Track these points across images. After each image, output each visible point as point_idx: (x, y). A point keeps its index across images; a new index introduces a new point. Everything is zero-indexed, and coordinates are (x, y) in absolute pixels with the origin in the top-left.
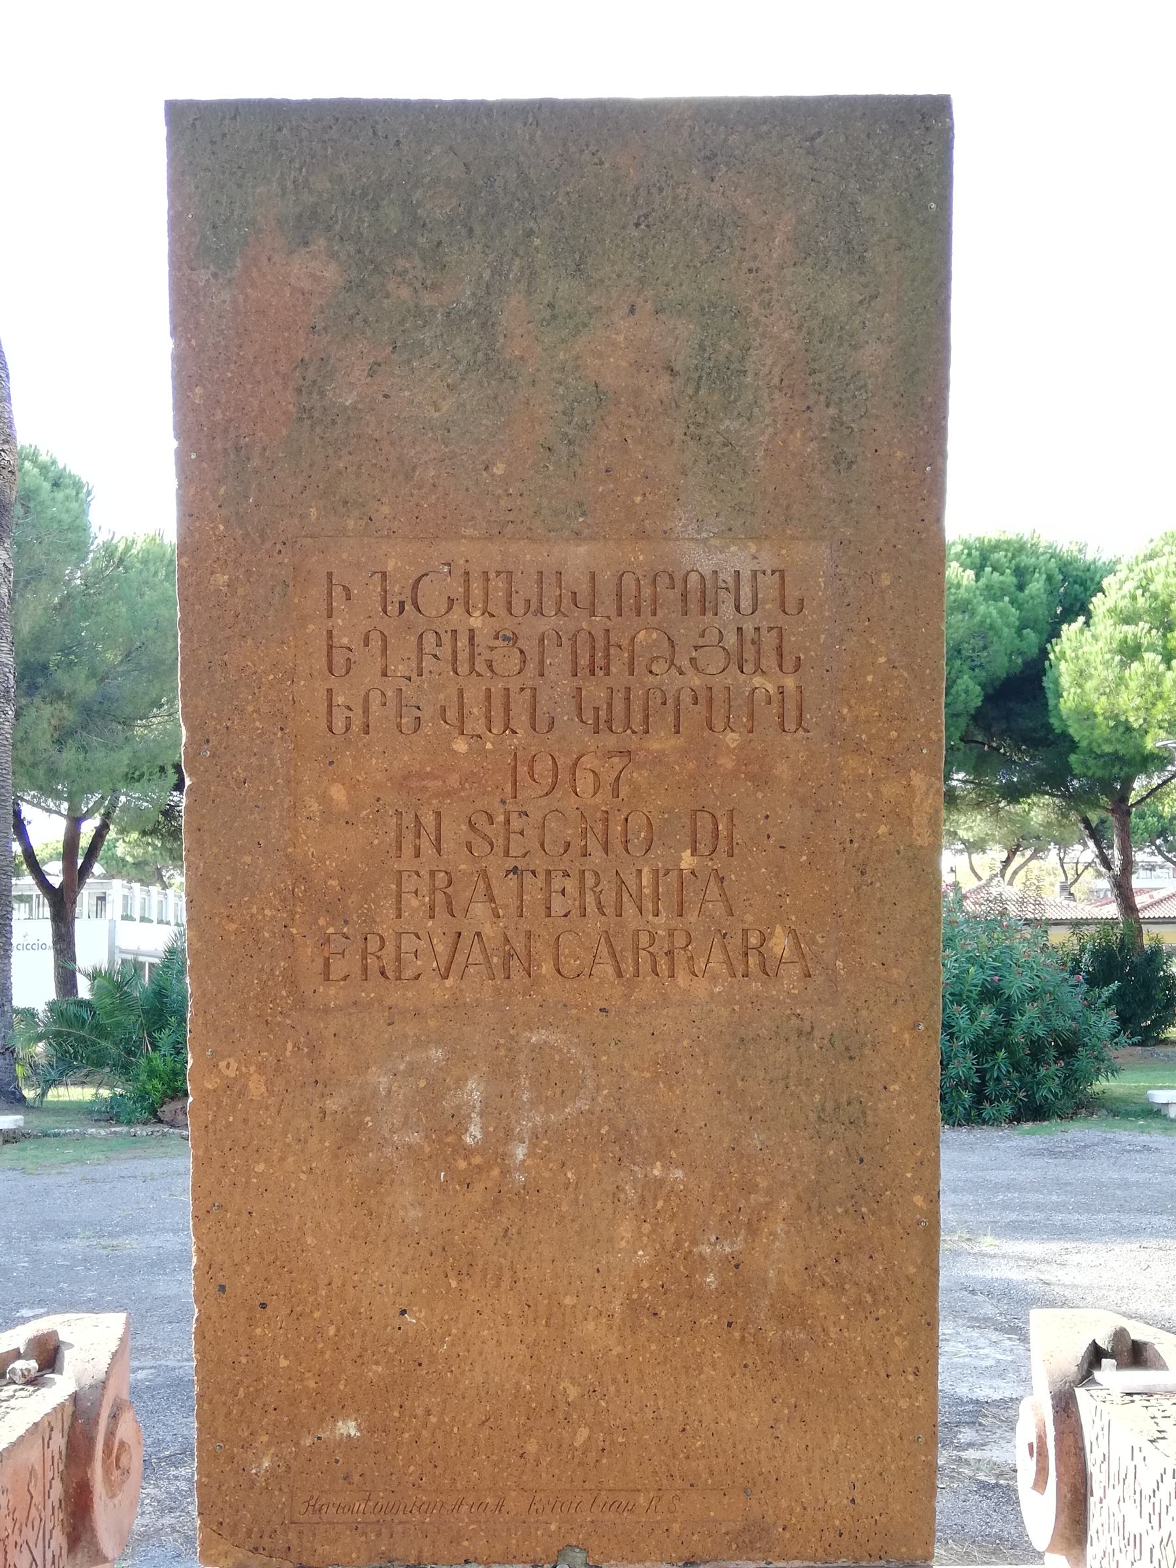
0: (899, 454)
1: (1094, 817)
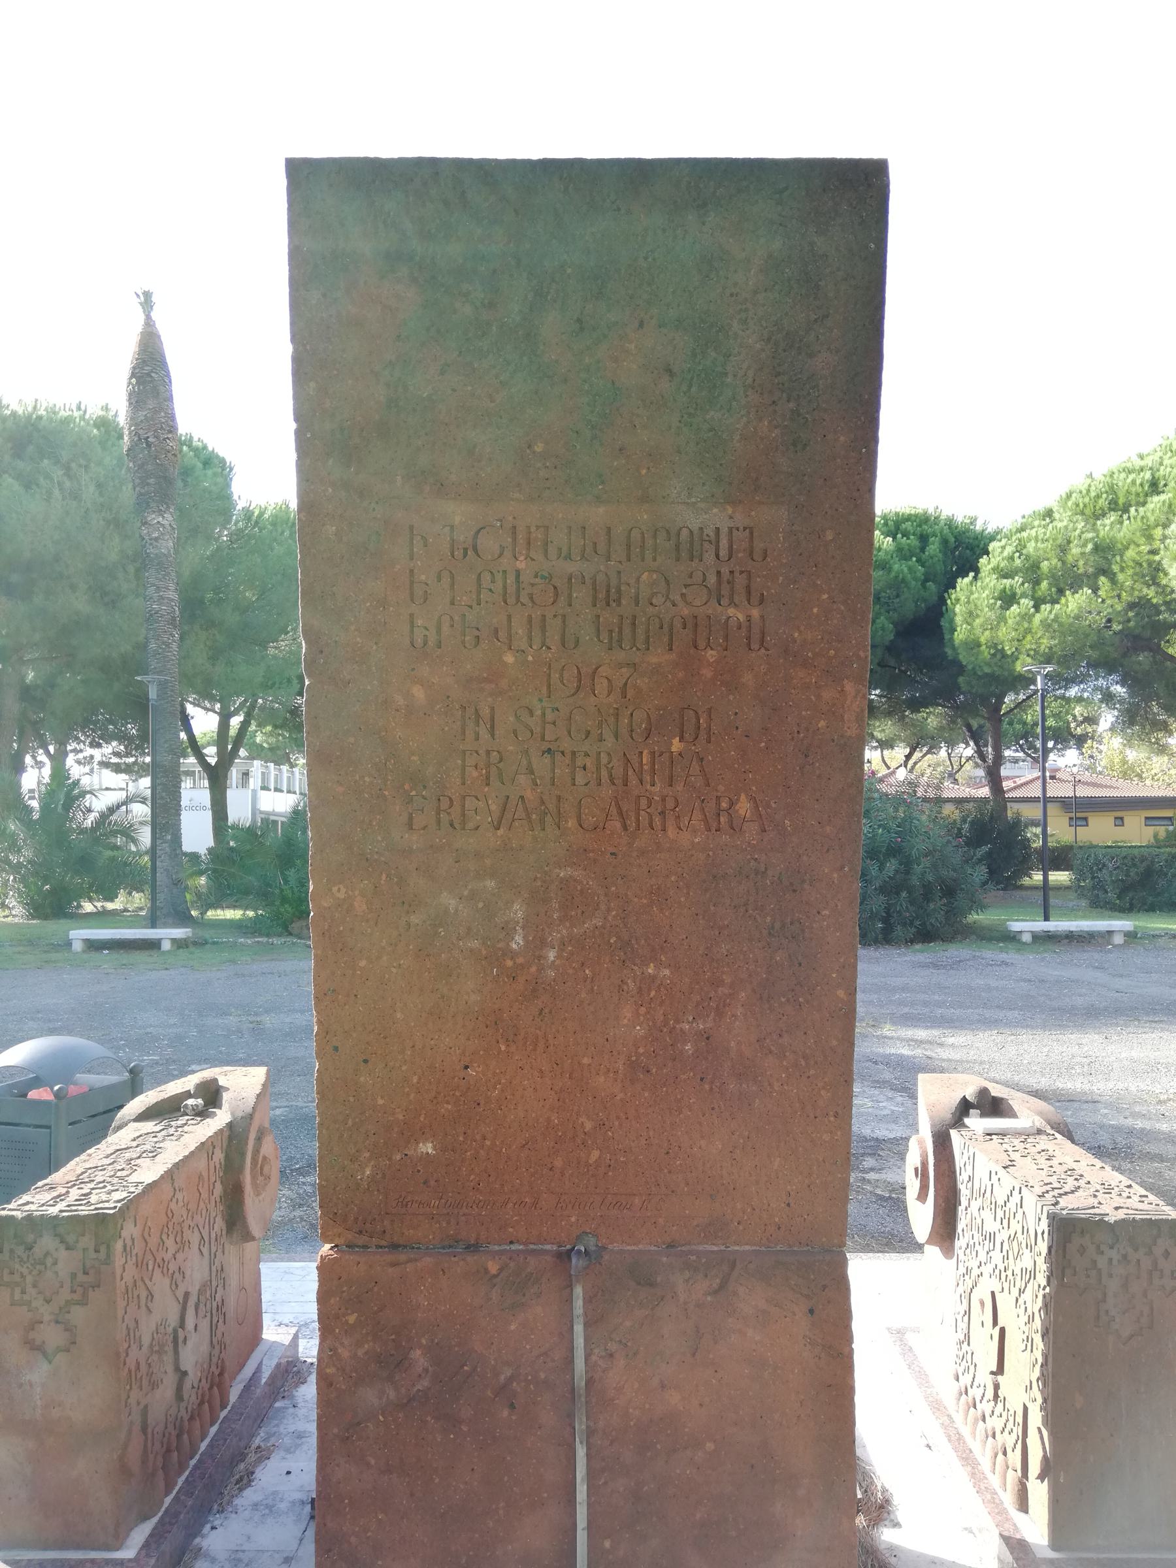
0: (842, 438)
1: (975, 724)
